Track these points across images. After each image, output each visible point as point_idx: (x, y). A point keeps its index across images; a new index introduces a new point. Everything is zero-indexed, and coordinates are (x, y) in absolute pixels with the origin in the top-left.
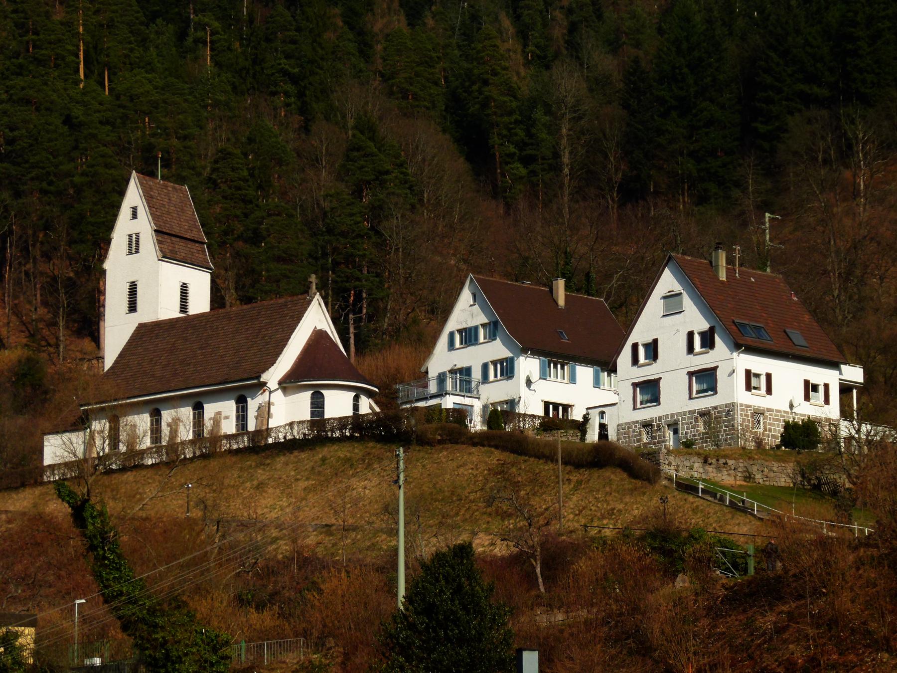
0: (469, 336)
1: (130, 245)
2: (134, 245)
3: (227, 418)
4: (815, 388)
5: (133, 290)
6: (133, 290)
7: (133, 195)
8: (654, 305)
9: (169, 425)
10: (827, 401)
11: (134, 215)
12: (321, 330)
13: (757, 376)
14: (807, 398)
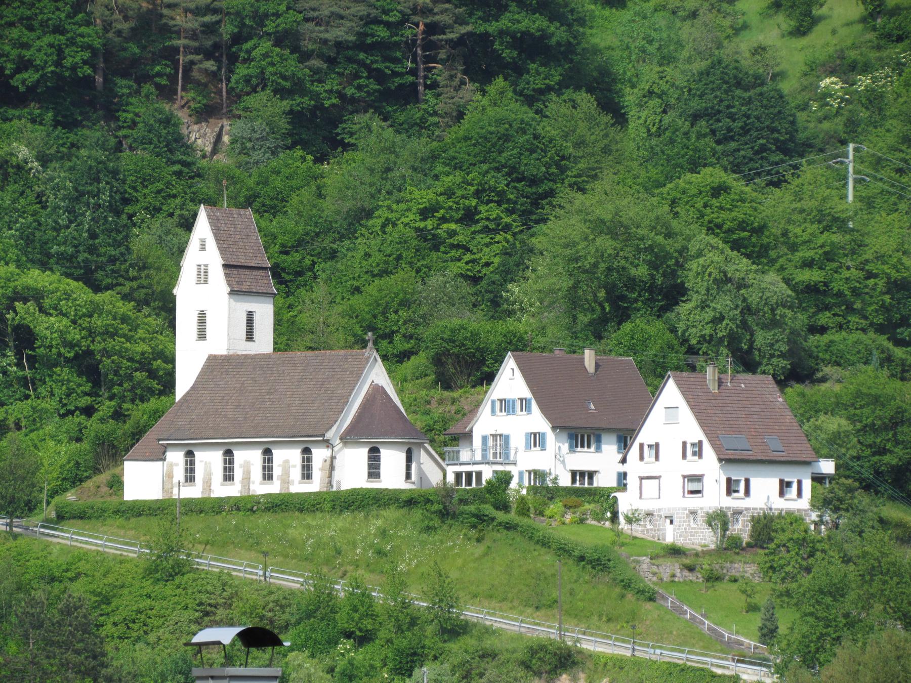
0: (507, 406)
1: (199, 274)
2: (203, 276)
3: (295, 466)
4: (789, 484)
5: (202, 319)
6: (202, 319)
7: (203, 227)
8: (657, 413)
9: (241, 466)
10: (800, 494)
11: (203, 247)
12: (377, 385)
13: (738, 481)
14: (782, 494)
